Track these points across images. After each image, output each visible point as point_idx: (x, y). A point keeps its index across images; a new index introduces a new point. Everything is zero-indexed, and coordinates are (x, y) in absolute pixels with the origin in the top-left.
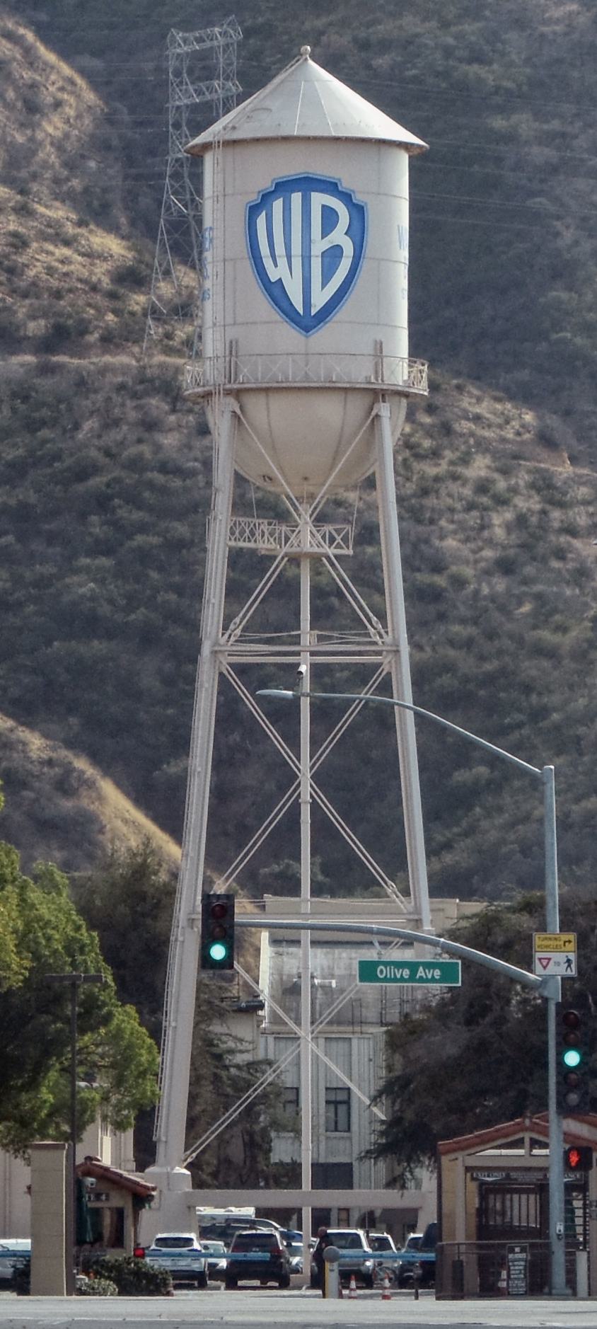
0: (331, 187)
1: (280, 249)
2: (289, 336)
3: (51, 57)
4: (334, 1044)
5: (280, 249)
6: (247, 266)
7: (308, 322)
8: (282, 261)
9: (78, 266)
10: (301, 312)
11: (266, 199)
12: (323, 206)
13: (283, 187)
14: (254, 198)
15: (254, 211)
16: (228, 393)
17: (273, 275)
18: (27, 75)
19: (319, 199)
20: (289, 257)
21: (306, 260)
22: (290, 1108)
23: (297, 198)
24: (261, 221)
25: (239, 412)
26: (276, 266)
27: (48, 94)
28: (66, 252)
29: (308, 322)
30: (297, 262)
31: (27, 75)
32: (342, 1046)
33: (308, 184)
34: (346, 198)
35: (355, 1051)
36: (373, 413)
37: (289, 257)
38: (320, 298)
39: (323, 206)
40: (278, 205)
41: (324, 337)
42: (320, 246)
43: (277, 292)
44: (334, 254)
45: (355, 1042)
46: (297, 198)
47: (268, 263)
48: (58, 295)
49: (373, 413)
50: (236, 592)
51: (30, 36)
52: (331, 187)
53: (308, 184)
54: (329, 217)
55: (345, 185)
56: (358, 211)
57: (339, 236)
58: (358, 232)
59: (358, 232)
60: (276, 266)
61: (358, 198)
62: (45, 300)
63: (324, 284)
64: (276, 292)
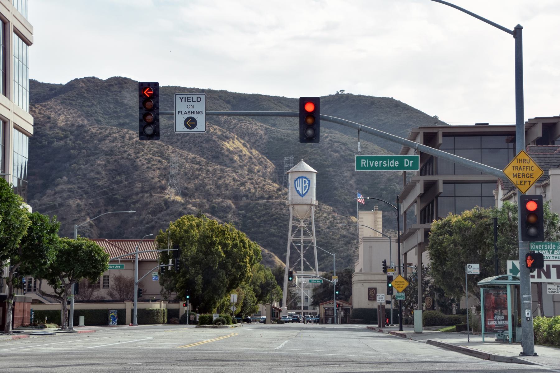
0: (305, 178)
2: (300, 197)
7: (302, 196)
9: (272, 188)
11: (297, 179)
13: (299, 178)
15: (295, 181)
19: (304, 179)
27: (268, 166)
29: (302, 196)
33: (302, 177)
34: (307, 179)
38: (304, 192)
41: (304, 198)
42: (304, 185)
44: (306, 187)
50: (293, 231)
52: (305, 178)
53: (302, 177)
54: (305, 182)
56: (309, 181)
57: (306, 184)
58: (309, 184)
59: (309, 184)
64: (298, 192)
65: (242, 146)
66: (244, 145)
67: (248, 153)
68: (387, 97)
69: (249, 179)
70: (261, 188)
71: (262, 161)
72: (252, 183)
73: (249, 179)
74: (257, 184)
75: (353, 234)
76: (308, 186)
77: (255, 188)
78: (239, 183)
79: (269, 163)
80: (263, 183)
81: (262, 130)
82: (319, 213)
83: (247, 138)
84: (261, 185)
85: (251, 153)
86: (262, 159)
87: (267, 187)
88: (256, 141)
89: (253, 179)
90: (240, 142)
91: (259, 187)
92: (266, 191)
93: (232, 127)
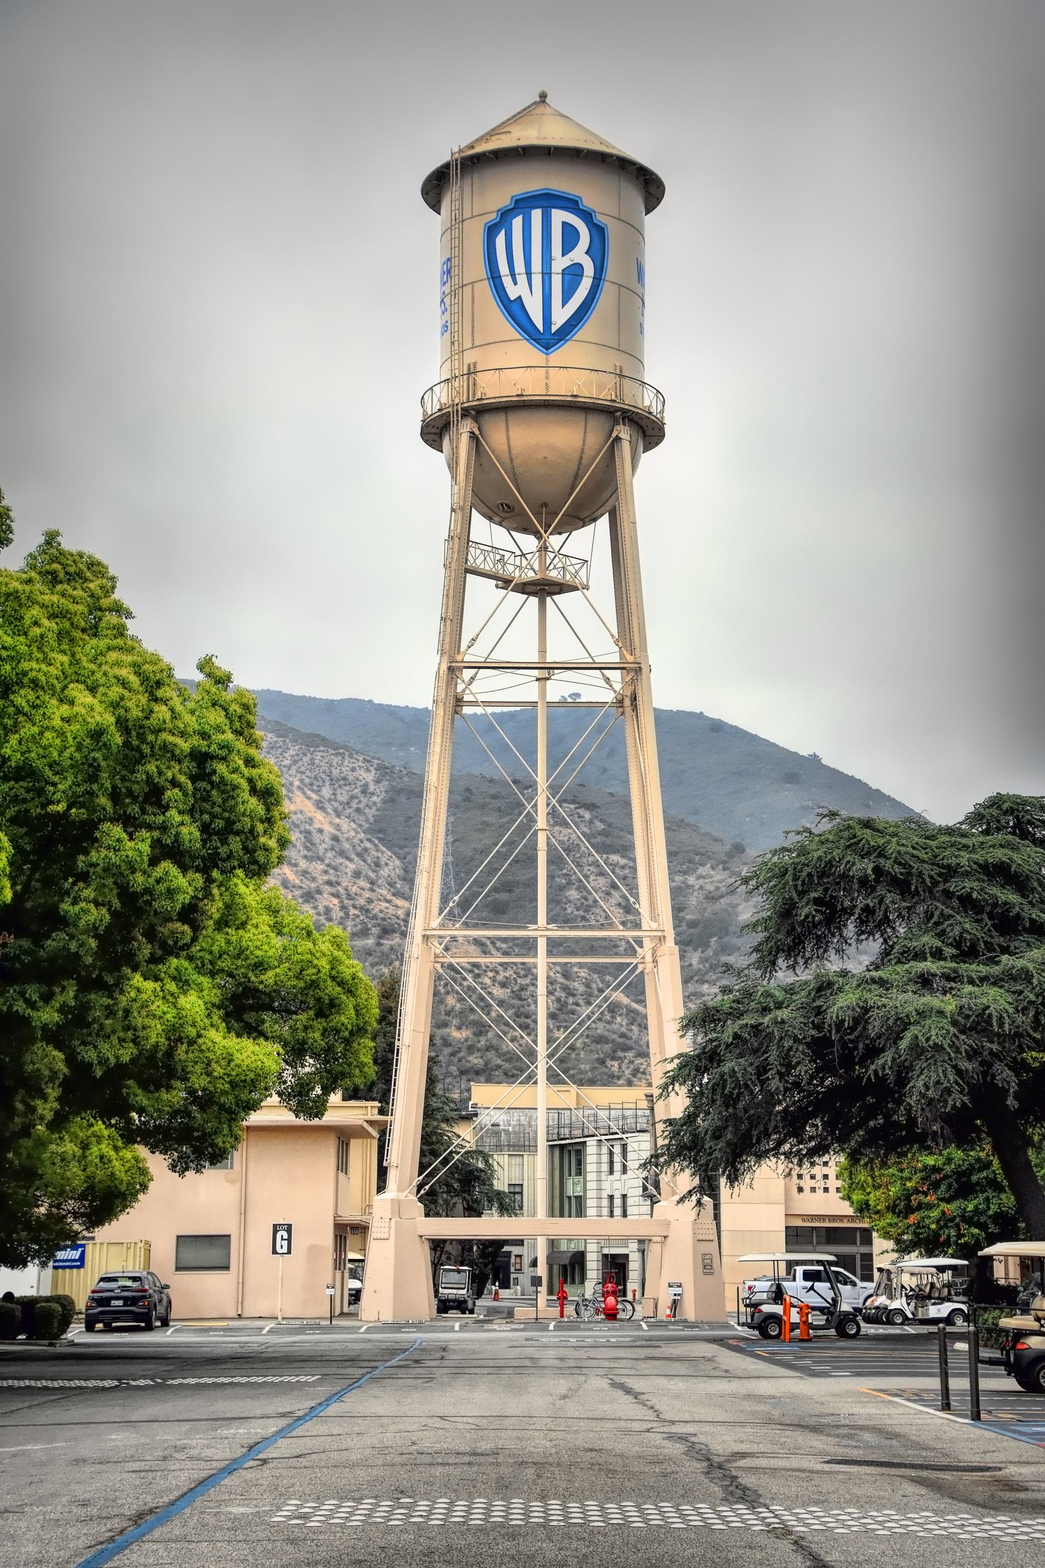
0: (572, 204)
1: (520, 266)
3: (384, 849)
4: (513, 1158)
5: (520, 266)
6: (485, 289)
8: (522, 279)
9: (391, 910)
10: (541, 329)
11: (505, 216)
12: (564, 223)
14: (493, 217)
15: (491, 231)
16: (466, 413)
17: (513, 292)
18: (376, 854)
19: (559, 216)
20: (529, 274)
21: (547, 277)
22: (448, 1248)
23: (537, 214)
24: (500, 240)
25: (477, 432)
26: (515, 283)
27: (383, 860)
28: (387, 905)
29: (548, 339)
30: (537, 279)
31: (376, 854)
32: (518, 1160)
33: (548, 200)
34: (587, 216)
35: (525, 1163)
36: (614, 435)
37: (529, 274)
38: (560, 316)
39: (564, 223)
40: (517, 222)
42: (560, 263)
43: (515, 308)
44: (574, 273)
45: (525, 1157)
46: (537, 214)
47: (507, 281)
48: (384, 919)
49: (614, 435)
51: (377, 842)
52: (572, 204)
53: (548, 200)
56: (599, 232)
57: (579, 255)
60: (515, 283)
62: (379, 921)
63: (564, 303)
64: (515, 311)
65: (313, 808)
66: (320, 806)
67: (328, 828)
68: (688, 709)
69: (329, 883)
70: (361, 908)
71: (366, 850)
72: (336, 895)
73: (329, 883)
74: (349, 897)
75: (623, 1035)
76: (589, 269)
77: (343, 907)
78: (298, 893)
79: (386, 855)
80: (367, 894)
81: (368, 770)
82: (526, 976)
83: (326, 792)
84: (361, 901)
85: (338, 827)
86: (368, 845)
87: (377, 907)
88: (352, 797)
89: (338, 884)
90: (309, 798)
91: (354, 907)
92: (375, 917)
93: (287, 762)
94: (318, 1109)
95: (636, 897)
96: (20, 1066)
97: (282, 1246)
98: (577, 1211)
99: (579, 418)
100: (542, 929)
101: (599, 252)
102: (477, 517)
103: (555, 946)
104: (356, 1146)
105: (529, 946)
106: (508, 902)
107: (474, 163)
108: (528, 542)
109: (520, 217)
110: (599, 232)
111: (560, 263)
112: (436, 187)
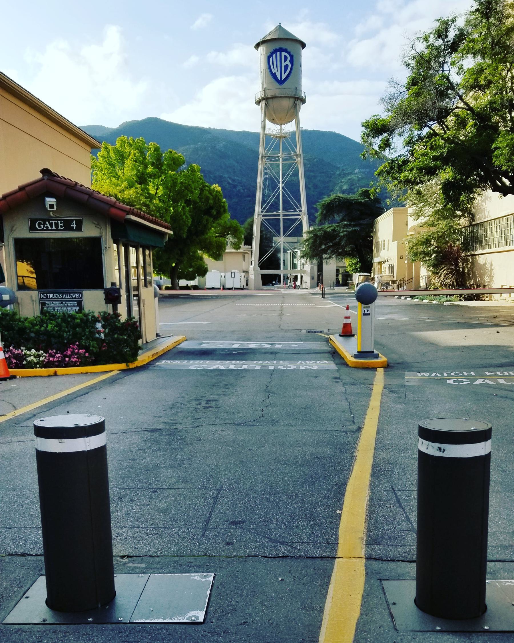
0: (286, 51)
19: (283, 54)
23: (278, 53)
34: (289, 53)
38: (284, 77)
40: (274, 55)
42: (283, 64)
44: (286, 67)
46: (278, 53)
52: (286, 51)
53: (281, 50)
54: (286, 58)
55: (289, 50)
56: (292, 57)
57: (288, 62)
61: (292, 53)
94: (239, 248)
95: (301, 206)
96: (492, 164)
97: (233, 276)
98: (378, 271)
99: (288, 99)
100: (281, 211)
101: (292, 61)
102: (267, 122)
103: (284, 215)
104: (246, 255)
105: (279, 215)
106: (275, 207)
107: (264, 42)
108: (278, 126)
109: (35, 277)
110: (292, 57)
111: (283, 64)
112: (258, 46)
